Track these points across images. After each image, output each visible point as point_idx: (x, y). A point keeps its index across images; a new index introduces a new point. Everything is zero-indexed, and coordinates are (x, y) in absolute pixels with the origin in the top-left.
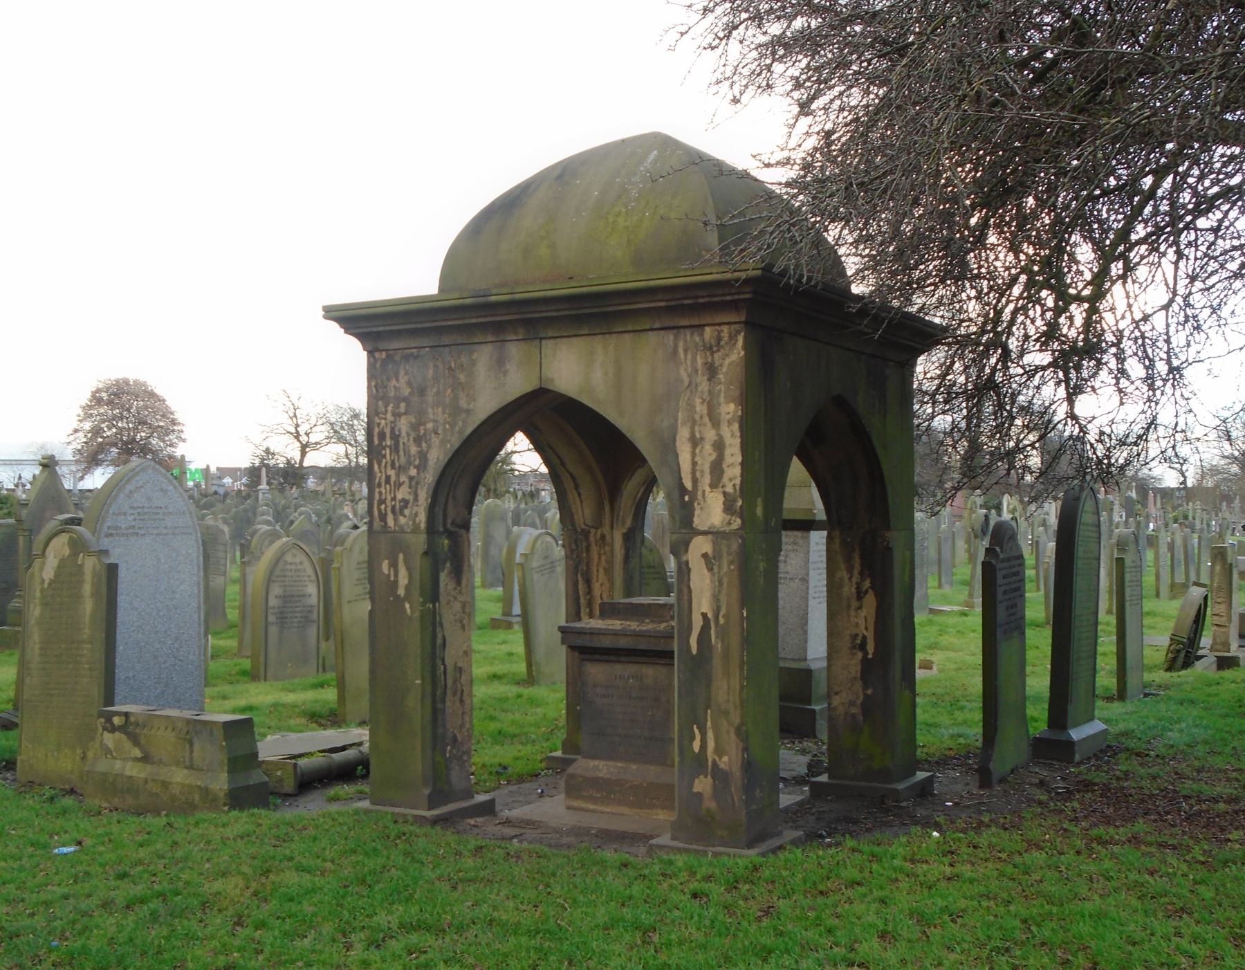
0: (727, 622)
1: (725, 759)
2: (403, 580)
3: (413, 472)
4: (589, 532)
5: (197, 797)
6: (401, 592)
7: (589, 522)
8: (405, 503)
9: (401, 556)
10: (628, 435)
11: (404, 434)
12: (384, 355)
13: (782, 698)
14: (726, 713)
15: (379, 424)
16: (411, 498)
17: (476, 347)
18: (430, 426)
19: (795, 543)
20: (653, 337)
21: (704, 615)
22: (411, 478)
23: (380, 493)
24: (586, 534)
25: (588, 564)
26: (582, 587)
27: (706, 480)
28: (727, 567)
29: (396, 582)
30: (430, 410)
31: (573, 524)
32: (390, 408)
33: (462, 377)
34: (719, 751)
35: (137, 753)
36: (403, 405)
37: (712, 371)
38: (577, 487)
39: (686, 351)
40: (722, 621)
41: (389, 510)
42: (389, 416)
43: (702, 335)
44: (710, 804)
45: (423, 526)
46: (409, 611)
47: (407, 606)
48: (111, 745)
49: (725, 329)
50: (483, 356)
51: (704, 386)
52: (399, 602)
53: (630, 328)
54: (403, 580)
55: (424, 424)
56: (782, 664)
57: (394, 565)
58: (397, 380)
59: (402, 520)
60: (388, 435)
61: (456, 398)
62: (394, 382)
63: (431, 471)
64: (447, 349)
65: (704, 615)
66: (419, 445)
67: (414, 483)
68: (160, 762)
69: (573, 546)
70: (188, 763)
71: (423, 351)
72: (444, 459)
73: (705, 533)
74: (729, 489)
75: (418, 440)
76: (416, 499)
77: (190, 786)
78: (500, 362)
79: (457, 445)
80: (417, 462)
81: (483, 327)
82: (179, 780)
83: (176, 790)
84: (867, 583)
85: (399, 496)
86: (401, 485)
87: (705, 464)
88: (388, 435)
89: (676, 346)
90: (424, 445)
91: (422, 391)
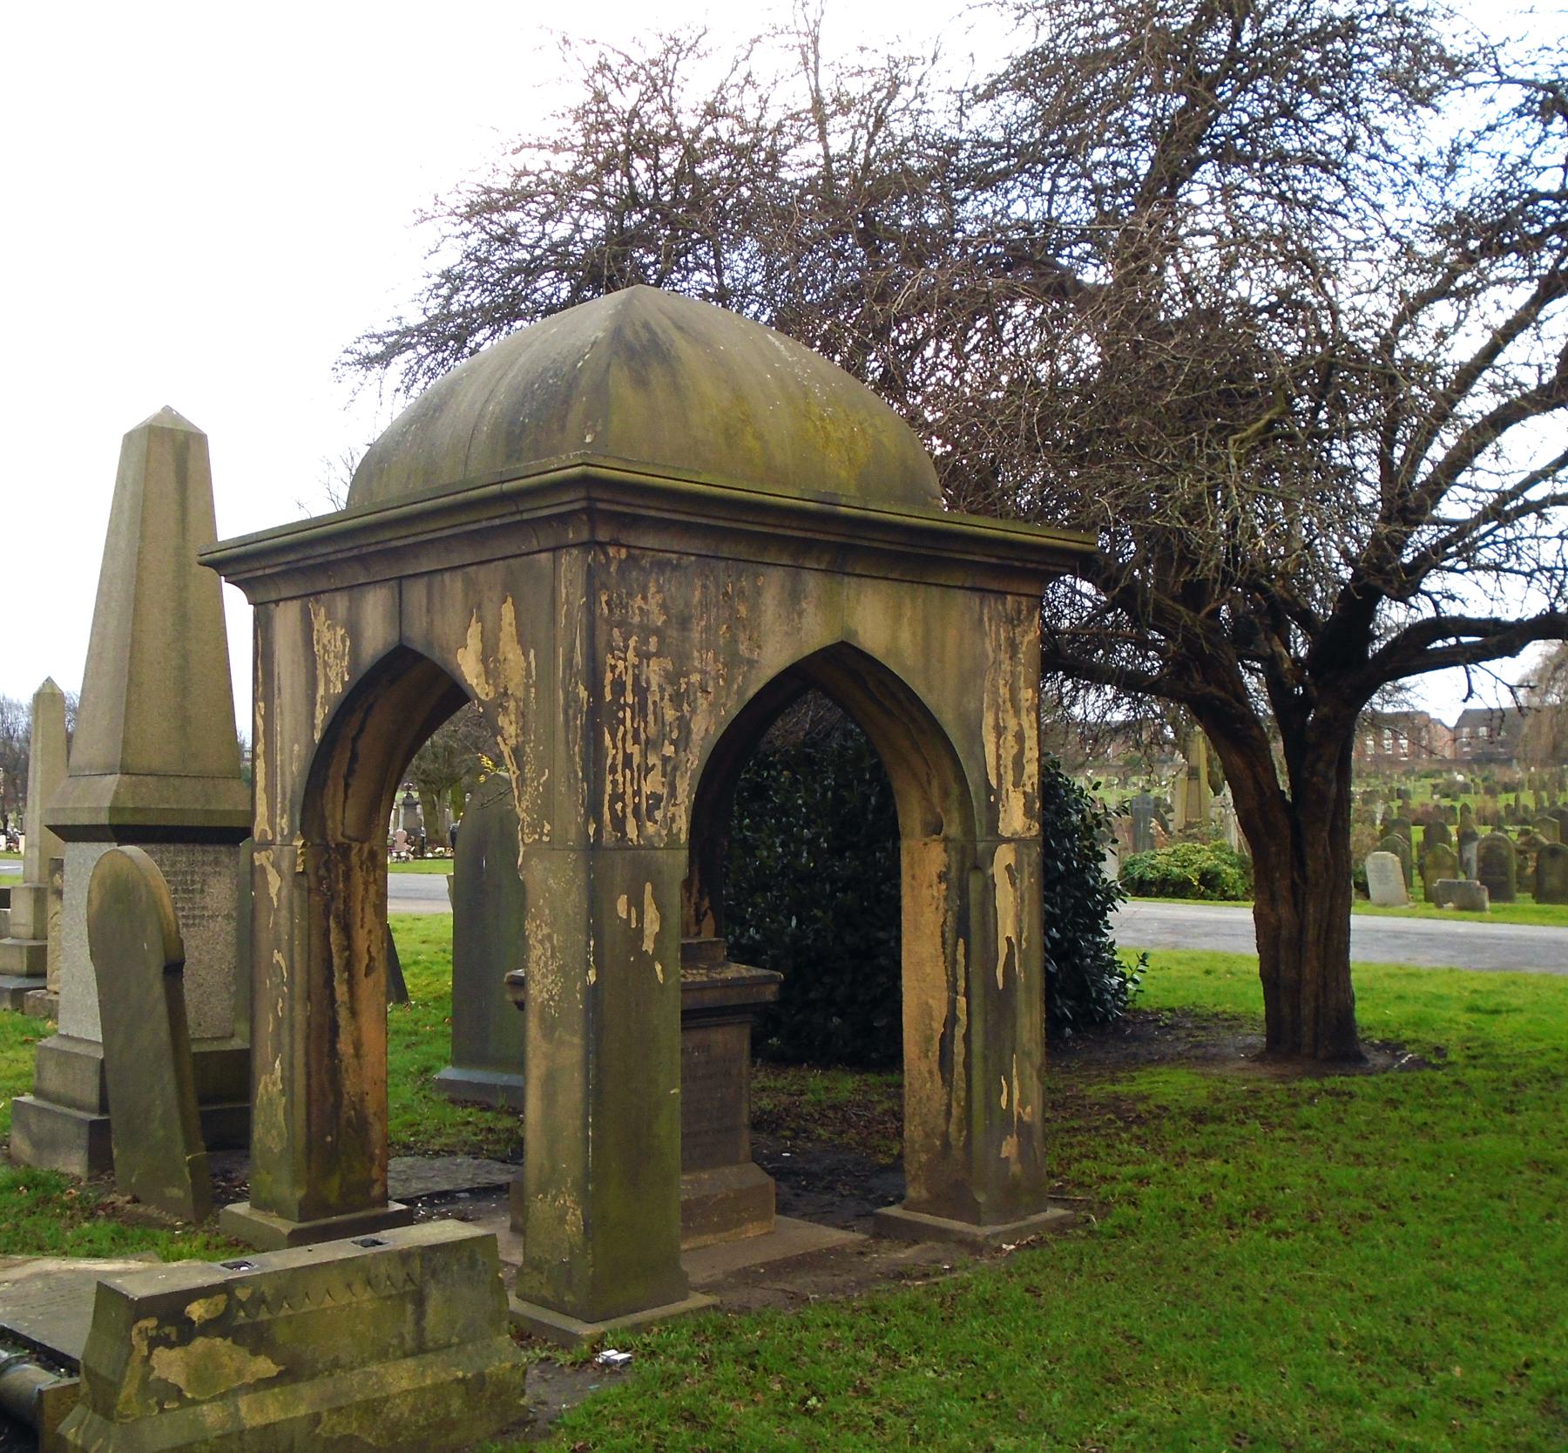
0: (1029, 946)
1: (1029, 1109)
2: (652, 925)
3: (669, 750)
4: (349, 848)
5: (456, 1404)
6: (648, 946)
7: (349, 832)
8: (656, 799)
9: (648, 887)
10: (937, 716)
11: (654, 687)
12: (623, 553)
13: (203, 1100)
14: (1029, 1055)
15: (613, 668)
16: (665, 792)
17: (762, 569)
18: (695, 678)
19: (217, 862)
20: (960, 597)
21: (1009, 939)
22: (665, 760)
23: (615, 783)
24: (344, 850)
25: (347, 900)
26: (335, 938)
27: (1009, 777)
28: (1029, 880)
29: (640, 930)
30: (696, 654)
31: (323, 835)
32: (632, 643)
33: (743, 611)
34: (1022, 1104)
35: (265, 1367)
36: (653, 640)
37: (1013, 647)
38: (350, 772)
39: (990, 620)
40: (1024, 945)
41: (629, 810)
42: (630, 654)
43: (1004, 604)
44: (1016, 1168)
45: (683, 837)
46: (660, 977)
47: (658, 968)
48: (176, 1376)
49: (1024, 600)
50: (772, 586)
51: (1006, 666)
52: (645, 961)
53: (942, 581)
54: (652, 925)
55: (686, 675)
56: (195, 1048)
57: (636, 903)
58: (645, 598)
59: (650, 828)
60: (629, 687)
61: (734, 641)
62: (639, 601)
63: (696, 750)
64: (722, 564)
65: (1009, 939)
66: (679, 708)
67: (671, 769)
68: (336, 1364)
69: (322, 872)
70: (410, 1343)
71: (685, 560)
72: (716, 732)
73: (1008, 841)
74: (1029, 789)
75: (677, 699)
76: (673, 793)
77: (437, 1387)
78: (794, 596)
79: (735, 713)
80: (675, 735)
81: (783, 542)
82: (405, 1384)
83: (400, 1410)
84: (706, 903)
85: (647, 789)
86: (649, 770)
87: (1008, 761)
88: (629, 687)
89: (982, 613)
90: (685, 707)
91: (684, 623)
